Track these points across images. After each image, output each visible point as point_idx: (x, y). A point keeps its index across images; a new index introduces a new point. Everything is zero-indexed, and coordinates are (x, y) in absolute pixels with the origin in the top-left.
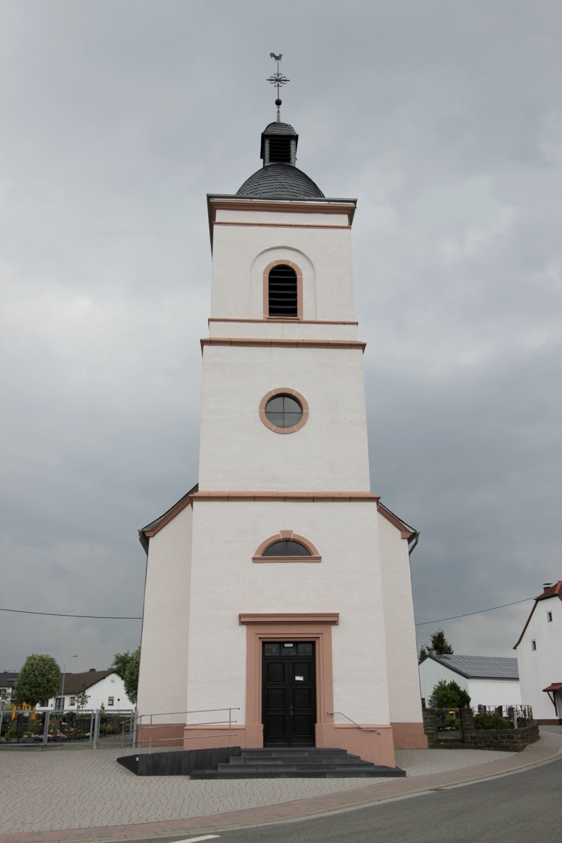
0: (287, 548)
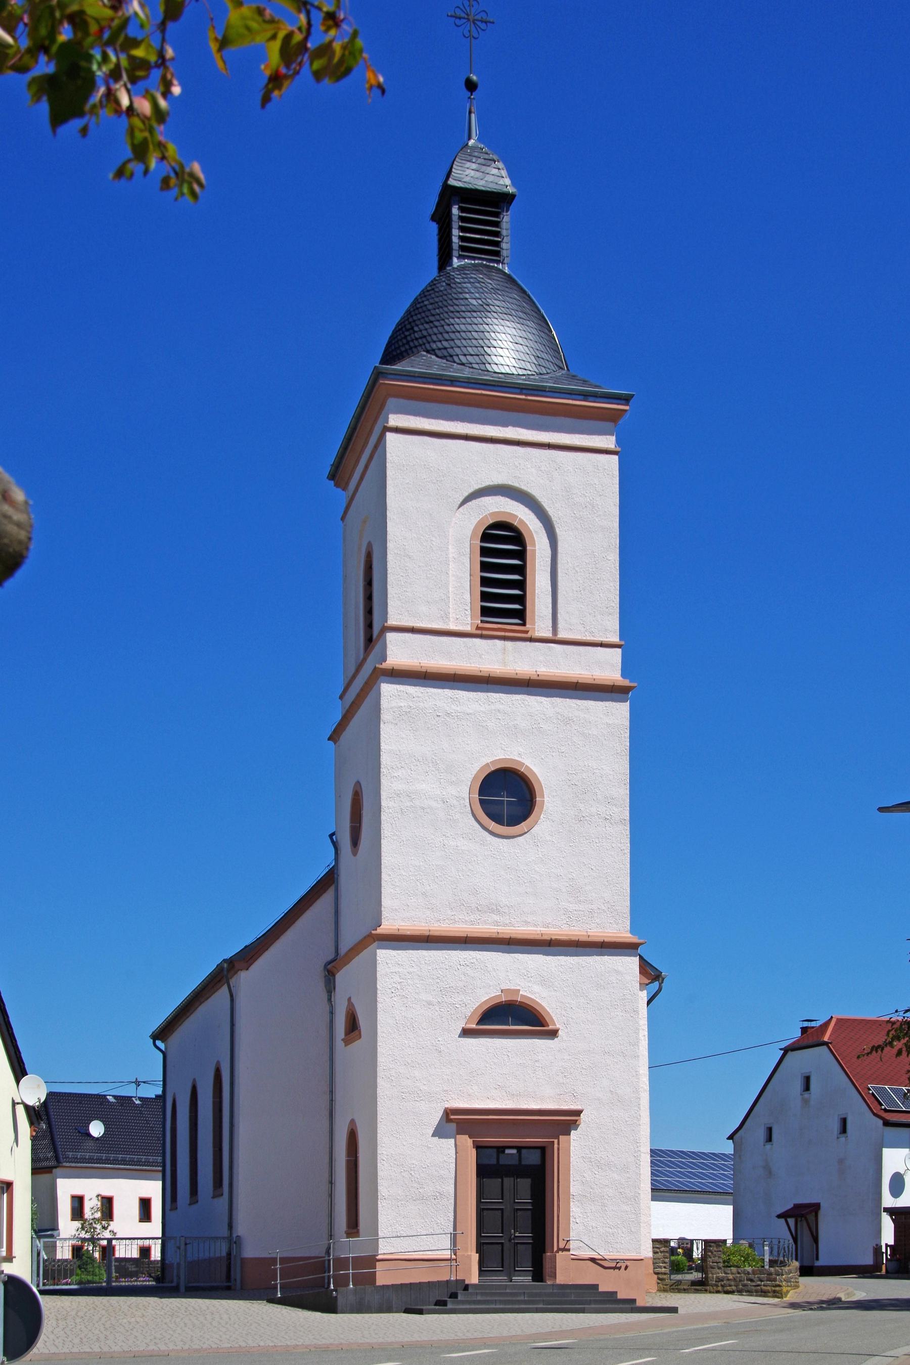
0: (513, 1017)
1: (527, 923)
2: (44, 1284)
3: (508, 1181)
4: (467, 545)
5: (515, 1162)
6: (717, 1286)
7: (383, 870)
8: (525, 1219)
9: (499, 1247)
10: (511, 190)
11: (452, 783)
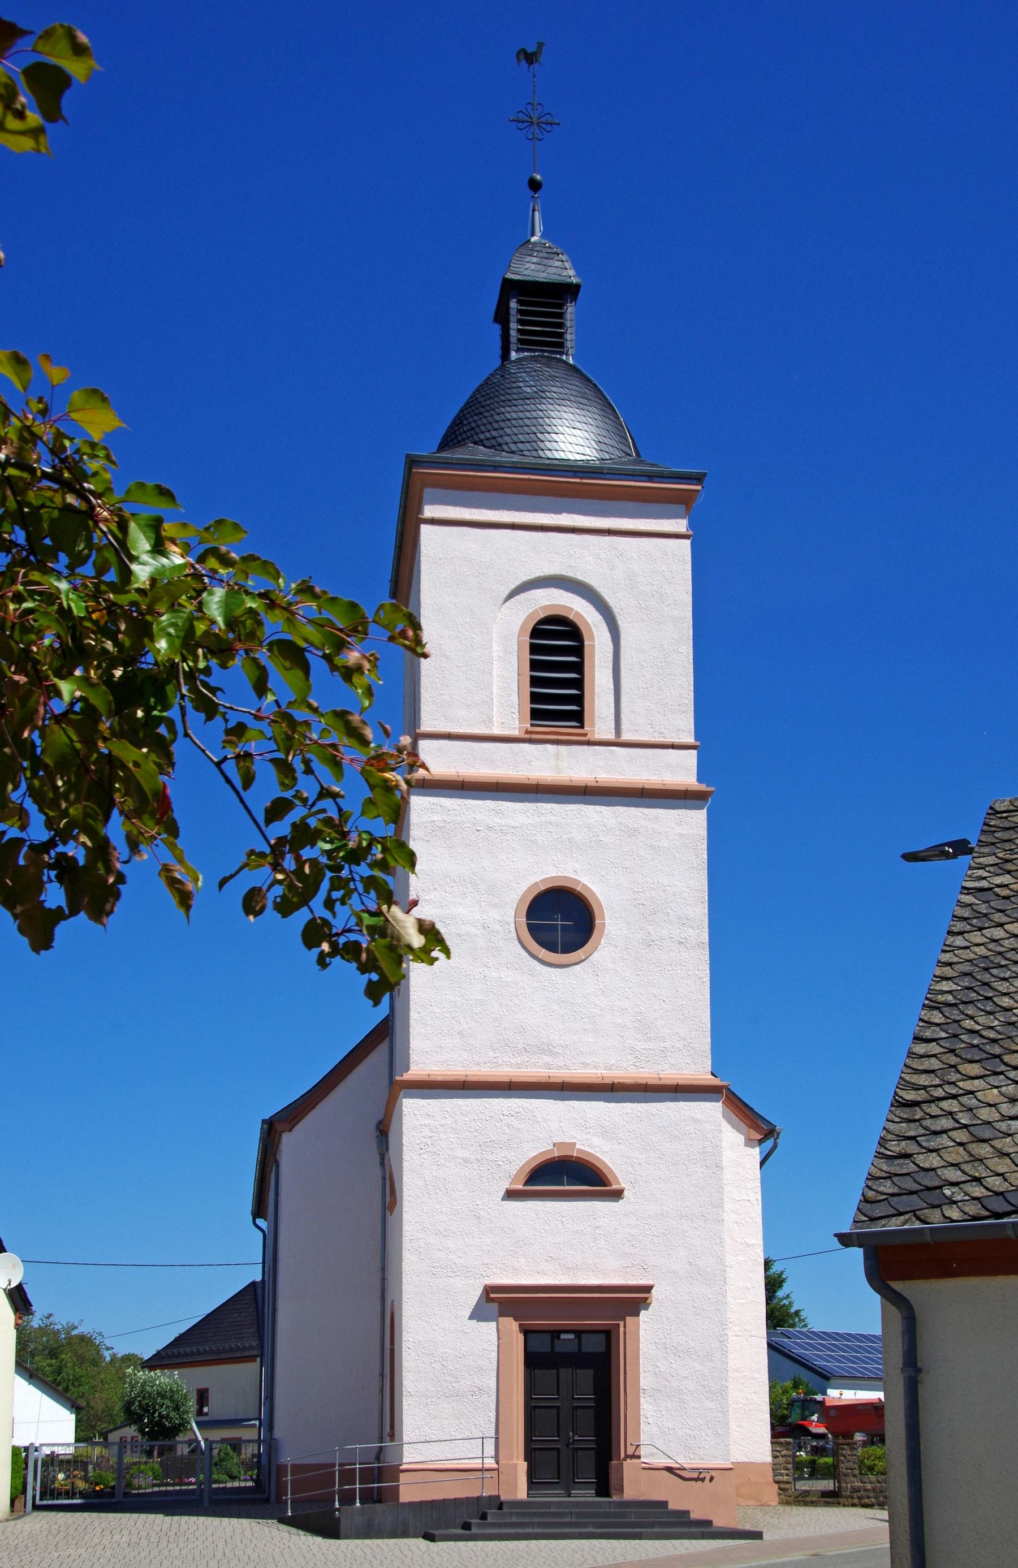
0: (564, 1175)
1: (586, 1065)
2: (41, 1499)
3: (565, 1373)
4: (515, 642)
5: (573, 1348)
6: (852, 1498)
7: (412, 1007)
8: (587, 1419)
9: (555, 1453)
10: (574, 280)
11: (495, 905)
